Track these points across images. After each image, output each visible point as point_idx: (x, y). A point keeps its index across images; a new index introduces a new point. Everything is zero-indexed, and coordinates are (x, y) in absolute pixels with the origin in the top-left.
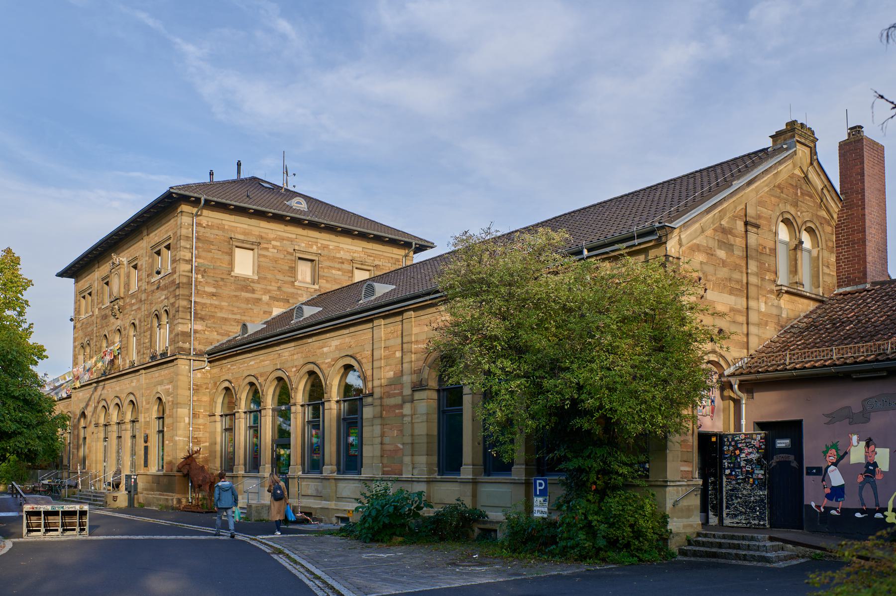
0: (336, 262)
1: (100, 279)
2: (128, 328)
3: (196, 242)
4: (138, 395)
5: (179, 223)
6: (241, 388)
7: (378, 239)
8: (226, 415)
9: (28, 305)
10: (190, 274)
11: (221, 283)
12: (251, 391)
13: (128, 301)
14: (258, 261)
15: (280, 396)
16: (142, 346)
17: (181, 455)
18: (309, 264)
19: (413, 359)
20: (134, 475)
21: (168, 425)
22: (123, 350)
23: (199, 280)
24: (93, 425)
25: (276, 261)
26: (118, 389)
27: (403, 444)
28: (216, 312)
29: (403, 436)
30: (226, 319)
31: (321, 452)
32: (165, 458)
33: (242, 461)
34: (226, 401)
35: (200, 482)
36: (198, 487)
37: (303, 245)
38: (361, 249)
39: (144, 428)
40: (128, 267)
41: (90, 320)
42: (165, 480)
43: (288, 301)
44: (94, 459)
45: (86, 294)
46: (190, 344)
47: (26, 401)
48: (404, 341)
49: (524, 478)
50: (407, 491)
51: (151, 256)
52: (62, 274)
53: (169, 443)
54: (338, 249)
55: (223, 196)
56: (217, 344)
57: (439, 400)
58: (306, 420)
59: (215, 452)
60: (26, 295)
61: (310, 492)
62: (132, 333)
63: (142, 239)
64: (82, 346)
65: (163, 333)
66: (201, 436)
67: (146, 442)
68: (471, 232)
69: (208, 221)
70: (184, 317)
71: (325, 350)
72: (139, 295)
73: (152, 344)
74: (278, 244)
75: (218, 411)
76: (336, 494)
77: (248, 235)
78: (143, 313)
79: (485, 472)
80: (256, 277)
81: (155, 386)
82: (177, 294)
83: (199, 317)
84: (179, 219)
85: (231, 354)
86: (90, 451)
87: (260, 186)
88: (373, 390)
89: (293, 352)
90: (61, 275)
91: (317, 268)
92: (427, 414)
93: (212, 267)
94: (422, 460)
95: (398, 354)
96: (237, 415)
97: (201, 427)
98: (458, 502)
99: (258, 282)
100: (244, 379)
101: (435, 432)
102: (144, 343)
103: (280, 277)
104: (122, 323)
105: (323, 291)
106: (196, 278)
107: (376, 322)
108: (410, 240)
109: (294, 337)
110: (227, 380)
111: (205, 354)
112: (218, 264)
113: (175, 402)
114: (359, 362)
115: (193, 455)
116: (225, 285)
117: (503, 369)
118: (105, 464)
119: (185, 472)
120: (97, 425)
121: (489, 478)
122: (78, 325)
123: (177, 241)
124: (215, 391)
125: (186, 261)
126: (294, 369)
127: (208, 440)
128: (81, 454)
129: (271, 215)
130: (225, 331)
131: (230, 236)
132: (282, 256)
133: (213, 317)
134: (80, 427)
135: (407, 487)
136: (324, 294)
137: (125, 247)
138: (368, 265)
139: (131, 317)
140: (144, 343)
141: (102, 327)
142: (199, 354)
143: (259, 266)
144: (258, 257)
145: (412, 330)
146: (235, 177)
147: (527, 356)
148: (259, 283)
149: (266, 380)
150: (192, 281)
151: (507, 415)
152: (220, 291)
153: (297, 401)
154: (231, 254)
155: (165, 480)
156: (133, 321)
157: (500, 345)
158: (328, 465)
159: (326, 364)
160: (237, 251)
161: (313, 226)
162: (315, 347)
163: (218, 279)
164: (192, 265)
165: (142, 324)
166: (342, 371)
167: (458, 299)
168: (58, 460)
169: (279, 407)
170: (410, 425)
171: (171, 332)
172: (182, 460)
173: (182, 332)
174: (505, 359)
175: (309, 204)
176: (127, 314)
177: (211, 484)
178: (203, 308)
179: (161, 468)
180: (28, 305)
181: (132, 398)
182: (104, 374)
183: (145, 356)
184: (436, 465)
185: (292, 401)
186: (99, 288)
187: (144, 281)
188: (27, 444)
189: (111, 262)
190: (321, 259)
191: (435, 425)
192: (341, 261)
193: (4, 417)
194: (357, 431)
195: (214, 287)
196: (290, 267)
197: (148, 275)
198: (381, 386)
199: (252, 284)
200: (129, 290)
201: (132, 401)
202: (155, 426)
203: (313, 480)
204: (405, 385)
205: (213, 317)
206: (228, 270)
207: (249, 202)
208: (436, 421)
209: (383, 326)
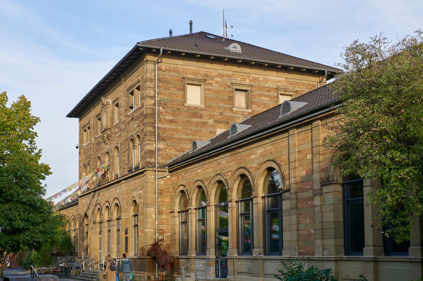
1: (95, 117)
2: (113, 150)
3: (157, 83)
4: (121, 200)
5: (145, 69)
6: (192, 190)
7: (297, 70)
8: (182, 212)
9: (37, 136)
10: (154, 107)
11: (177, 112)
12: (199, 193)
13: (113, 130)
14: (205, 94)
15: (220, 195)
16: (123, 163)
17: (152, 242)
18: (244, 93)
19: (321, 160)
20: (118, 259)
21: (140, 220)
22: (110, 167)
23: (160, 111)
24: (92, 223)
25: (218, 93)
26: (107, 195)
27: (315, 230)
28: (174, 134)
29: (315, 223)
30: (181, 139)
31: (251, 238)
32: (139, 245)
33: (194, 246)
34: (182, 201)
35: (163, 263)
36: (162, 267)
37: (239, 79)
38: (284, 79)
39: (125, 223)
40: (113, 106)
41: (89, 146)
42: (139, 262)
43: (228, 123)
44: (93, 247)
45: (86, 128)
46: (155, 159)
47: (31, 205)
48: (313, 145)
49: (420, 257)
50: (316, 269)
51: (127, 96)
52: (70, 115)
53: (142, 234)
55: (177, 47)
56: (175, 158)
57: (344, 192)
58: (240, 213)
59: (175, 240)
60: (36, 129)
61: (243, 270)
62: (116, 154)
63: (121, 84)
64: (85, 166)
65: (137, 152)
66: (164, 228)
67: (126, 233)
68: (360, 42)
69: (166, 67)
71: (252, 157)
72: (120, 125)
73: (129, 161)
74: (219, 80)
75: (177, 209)
76: (263, 272)
77: (197, 74)
78: (123, 138)
79: (385, 252)
80: (203, 106)
81: (131, 192)
82: (145, 122)
83: (161, 139)
84: (145, 66)
85: (184, 164)
86: (90, 242)
87: (206, 38)
88: (289, 186)
89: (228, 160)
90: (70, 116)
91: (250, 96)
92: (334, 204)
93: (170, 100)
94: (330, 242)
95: (309, 156)
96: (189, 211)
97: (165, 221)
98: (361, 278)
99: (205, 110)
100: (194, 184)
101: (341, 219)
102: (124, 161)
103: (222, 105)
104: (109, 147)
105: (255, 114)
106: (159, 110)
107: (291, 132)
108: (323, 69)
109: (229, 148)
110: (182, 185)
111: (167, 166)
112: (175, 98)
113: (145, 203)
114: (278, 165)
115: (158, 242)
116: (180, 114)
117: (392, 159)
118: (101, 251)
119: (153, 255)
120: (95, 223)
121: (388, 257)
122: (82, 151)
123: (144, 83)
124: (174, 193)
125: (151, 97)
126: (230, 174)
127: (170, 231)
128: (85, 244)
129: (213, 57)
130: (181, 148)
131: (182, 77)
134: (84, 225)
135: (317, 265)
136: (256, 115)
137: (111, 91)
138: (290, 91)
139: (115, 142)
140: (124, 161)
141: (97, 151)
142: (162, 166)
144: (205, 91)
145: (320, 136)
146: (188, 32)
147: (415, 146)
149: (209, 183)
150: (155, 112)
151: (397, 200)
152: (177, 118)
153: (233, 198)
154: (184, 90)
155: (139, 262)
156: (116, 145)
157: (390, 138)
158: (256, 248)
159: (254, 168)
160: (189, 87)
161: (246, 64)
162: (245, 156)
164: (155, 100)
165: (123, 147)
166: (266, 173)
167: (350, 100)
168: (72, 249)
169: (220, 204)
170: (320, 214)
171: (141, 151)
172: (151, 246)
173: (149, 150)
174: (394, 150)
175: (243, 48)
176: (112, 140)
177: (171, 265)
179: (137, 253)
180: (37, 136)
181: (116, 201)
182: (99, 185)
183: (125, 170)
184: (343, 247)
185: (229, 199)
186: (94, 124)
187: (123, 115)
188: (32, 237)
189: (101, 104)
190: (253, 89)
191: (341, 213)
192: (268, 89)
193: (15, 218)
194: (278, 220)
195: (172, 116)
196: (229, 97)
197: (126, 111)
198: (296, 183)
199: (200, 112)
200: (113, 123)
201: (117, 204)
202: (132, 222)
203: (246, 260)
204: (315, 181)
206: (182, 102)
207: (197, 49)
208: (342, 210)
209: (296, 135)
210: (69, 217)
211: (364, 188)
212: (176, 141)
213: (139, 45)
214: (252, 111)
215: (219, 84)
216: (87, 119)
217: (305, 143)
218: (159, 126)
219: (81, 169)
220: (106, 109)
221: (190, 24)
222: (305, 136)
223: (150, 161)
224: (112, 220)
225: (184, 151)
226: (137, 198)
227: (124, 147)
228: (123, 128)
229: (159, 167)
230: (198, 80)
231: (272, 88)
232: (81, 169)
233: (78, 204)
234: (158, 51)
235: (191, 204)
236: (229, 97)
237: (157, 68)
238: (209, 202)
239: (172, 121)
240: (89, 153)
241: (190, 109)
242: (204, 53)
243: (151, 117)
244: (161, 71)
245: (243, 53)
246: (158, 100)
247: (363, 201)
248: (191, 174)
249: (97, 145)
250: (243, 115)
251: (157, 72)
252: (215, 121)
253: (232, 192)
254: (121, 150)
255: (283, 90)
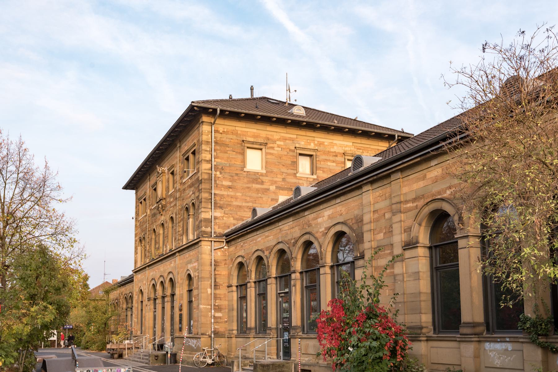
0: (330, 155)
3: (214, 146)
4: (175, 273)
5: (201, 131)
11: (236, 178)
14: (266, 158)
18: (308, 158)
25: (280, 158)
26: (162, 270)
28: (232, 202)
30: (240, 207)
37: (303, 143)
38: (351, 144)
39: (179, 299)
40: (168, 174)
41: (145, 219)
45: (142, 200)
52: (126, 187)
54: (333, 145)
56: (233, 228)
57: (431, 257)
69: (224, 129)
70: (206, 206)
71: (320, 220)
75: (235, 282)
77: (257, 137)
78: (178, 208)
80: (264, 171)
82: (200, 188)
83: (218, 206)
93: (228, 165)
96: (249, 285)
102: (179, 231)
103: (284, 170)
105: (320, 180)
106: (215, 175)
108: (393, 133)
112: (233, 162)
116: (239, 179)
122: (138, 224)
123: (200, 146)
124: (231, 266)
129: (275, 119)
131: (242, 140)
132: (286, 153)
133: (230, 205)
139: (170, 213)
140: (179, 231)
141: (152, 223)
142: (221, 236)
143: (266, 162)
144: (266, 155)
146: (249, 96)
148: (267, 176)
149: (270, 253)
150: (212, 177)
152: (235, 184)
154: (243, 154)
159: (321, 232)
163: (233, 175)
164: (212, 164)
165: (177, 216)
173: (205, 219)
176: (168, 210)
178: (221, 198)
181: (171, 276)
185: (292, 269)
186: (150, 194)
187: (178, 182)
190: (318, 153)
192: (335, 154)
195: (230, 181)
196: (292, 162)
199: (261, 177)
200: (169, 192)
205: (230, 205)
210: (127, 294)
211: (459, 251)
212: (234, 209)
213: (193, 104)
214: (317, 177)
215: (282, 148)
216: (143, 190)
217: (382, 200)
218: (216, 193)
219: (137, 243)
220: (162, 178)
221: (251, 89)
222: (382, 192)
223: (205, 230)
224: (166, 296)
225: (243, 219)
226: (191, 271)
227: (179, 217)
228: (178, 197)
229: (216, 237)
230: (258, 143)
231: (339, 153)
232: (137, 243)
233: (133, 281)
234: (215, 110)
235: (251, 276)
236: (292, 162)
237: (214, 130)
238: (270, 274)
239: (230, 187)
240: (144, 226)
241: (250, 174)
242: (265, 114)
243: (207, 183)
244: (218, 133)
245: (307, 116)
246: (215, 164)
247: (459, 266)
248: (251, 243)
249: (152, 217)
250: (307, 181)
251: (214, 135)
252: (277, 187)
253: (296, 261)
254: (176, 220)
255: (350, 155)
